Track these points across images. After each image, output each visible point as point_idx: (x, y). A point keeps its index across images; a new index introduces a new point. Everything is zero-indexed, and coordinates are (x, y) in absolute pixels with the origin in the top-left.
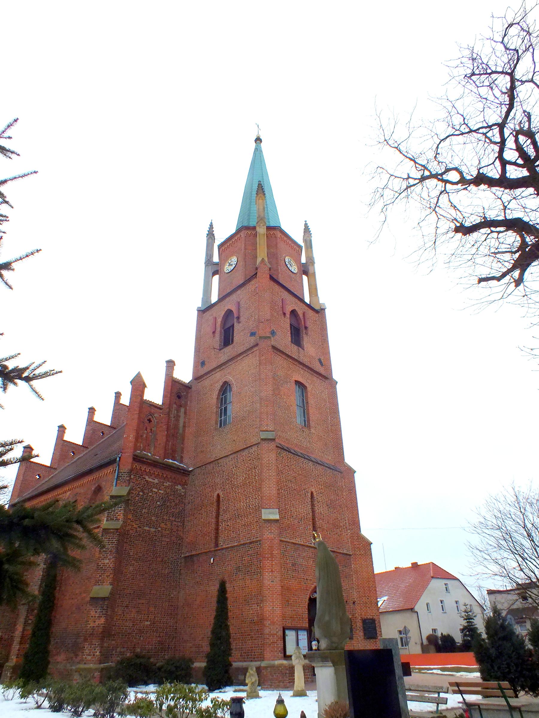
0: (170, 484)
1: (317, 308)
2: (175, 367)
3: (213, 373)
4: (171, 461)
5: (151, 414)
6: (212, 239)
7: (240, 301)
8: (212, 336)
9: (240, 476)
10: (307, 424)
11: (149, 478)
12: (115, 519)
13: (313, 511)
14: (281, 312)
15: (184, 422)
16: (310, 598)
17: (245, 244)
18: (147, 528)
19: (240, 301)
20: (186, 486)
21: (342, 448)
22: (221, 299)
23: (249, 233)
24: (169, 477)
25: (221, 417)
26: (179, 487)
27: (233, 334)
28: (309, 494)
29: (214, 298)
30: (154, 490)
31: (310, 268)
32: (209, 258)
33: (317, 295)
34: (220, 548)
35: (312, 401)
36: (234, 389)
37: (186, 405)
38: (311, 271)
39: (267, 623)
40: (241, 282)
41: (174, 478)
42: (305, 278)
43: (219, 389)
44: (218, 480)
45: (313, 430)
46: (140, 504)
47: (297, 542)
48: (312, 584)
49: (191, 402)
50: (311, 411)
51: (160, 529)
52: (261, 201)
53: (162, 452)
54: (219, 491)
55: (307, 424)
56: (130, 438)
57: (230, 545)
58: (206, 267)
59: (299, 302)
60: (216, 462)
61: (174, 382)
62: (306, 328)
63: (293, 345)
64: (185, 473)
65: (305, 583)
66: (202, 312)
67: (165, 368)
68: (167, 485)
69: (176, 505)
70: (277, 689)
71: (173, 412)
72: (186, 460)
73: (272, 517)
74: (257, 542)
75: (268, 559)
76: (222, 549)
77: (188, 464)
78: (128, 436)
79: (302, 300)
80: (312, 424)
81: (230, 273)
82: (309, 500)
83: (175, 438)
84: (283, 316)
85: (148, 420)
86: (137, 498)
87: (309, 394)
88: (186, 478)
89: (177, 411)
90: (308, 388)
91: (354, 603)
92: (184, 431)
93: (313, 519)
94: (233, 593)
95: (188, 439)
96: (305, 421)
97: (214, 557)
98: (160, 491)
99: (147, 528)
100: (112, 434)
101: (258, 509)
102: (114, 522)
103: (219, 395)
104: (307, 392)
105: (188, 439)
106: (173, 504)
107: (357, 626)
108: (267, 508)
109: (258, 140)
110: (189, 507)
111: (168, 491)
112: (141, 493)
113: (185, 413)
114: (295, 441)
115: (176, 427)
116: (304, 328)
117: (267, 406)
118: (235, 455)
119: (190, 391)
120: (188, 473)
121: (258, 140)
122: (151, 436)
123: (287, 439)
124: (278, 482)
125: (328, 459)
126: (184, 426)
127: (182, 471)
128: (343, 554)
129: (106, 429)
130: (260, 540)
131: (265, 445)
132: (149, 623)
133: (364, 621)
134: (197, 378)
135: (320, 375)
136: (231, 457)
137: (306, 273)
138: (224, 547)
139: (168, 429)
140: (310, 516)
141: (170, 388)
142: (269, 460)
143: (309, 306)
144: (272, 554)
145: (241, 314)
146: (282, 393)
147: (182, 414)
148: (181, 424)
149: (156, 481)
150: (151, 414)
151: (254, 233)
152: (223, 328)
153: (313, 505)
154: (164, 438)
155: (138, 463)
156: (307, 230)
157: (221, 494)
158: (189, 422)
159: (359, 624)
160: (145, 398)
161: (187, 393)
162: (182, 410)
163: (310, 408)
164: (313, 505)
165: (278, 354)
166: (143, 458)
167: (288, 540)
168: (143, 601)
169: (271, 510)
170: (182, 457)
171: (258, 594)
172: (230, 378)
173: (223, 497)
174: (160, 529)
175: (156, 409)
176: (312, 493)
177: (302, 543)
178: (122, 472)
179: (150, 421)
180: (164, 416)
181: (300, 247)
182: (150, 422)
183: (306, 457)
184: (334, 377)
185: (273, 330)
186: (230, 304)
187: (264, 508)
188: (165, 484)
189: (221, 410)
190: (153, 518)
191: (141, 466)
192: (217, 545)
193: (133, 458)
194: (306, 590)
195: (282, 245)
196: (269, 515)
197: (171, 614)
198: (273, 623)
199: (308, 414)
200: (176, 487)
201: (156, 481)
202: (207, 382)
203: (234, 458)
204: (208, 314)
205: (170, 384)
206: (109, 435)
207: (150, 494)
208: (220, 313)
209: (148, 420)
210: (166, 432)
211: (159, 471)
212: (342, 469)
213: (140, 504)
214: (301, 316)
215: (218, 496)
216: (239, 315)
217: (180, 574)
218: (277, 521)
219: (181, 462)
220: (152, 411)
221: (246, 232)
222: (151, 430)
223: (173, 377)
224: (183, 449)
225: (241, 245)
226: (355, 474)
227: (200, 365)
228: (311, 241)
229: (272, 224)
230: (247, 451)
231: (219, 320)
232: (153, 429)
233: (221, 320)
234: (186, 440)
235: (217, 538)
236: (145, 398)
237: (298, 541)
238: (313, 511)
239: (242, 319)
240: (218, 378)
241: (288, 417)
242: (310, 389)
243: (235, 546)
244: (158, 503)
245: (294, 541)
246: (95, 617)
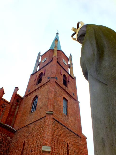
0: (5, 135)
1: (73, 77)
2: (18, 90)
4: (8, 125)
5: (4, 105)
10: (67, 114)
15: (18, 111)
17: (50, 54)
20: (12, 138)
21: (81, 127)
22: (39, 70)
25: (32, 109)
26: (9, 138)
28: (66, 144)
29: (38, 70)
33: (73, 73)
35: (69, 106)
36: (39, 97)
37: (20, 104)
41: (8, 133)
42: (69, 69)
44: (26, 134)
45: (69, 117)
49: (22, 104)
50: (69, 110)
52: (56, 42)
53: (5, 121)
54: (26, 140)
55: (67, 114)
59: (67, 73)
60: (27, 126)
61: (16, 95)
62: (69, 81)
63: (63, 85)
64: (14, 132)
66: (32, 75)
67: (14, 89)
68: (3, 135)
69: (5, 146)
70: (98, 87)
71: (14, 106)
72: (15, 126)
73: (47, 150)
77: (15, 128)
79: (68, 73)
80: (69, 115)
82: (66, 147)
83: (12, 117)
87: (69, 103)
89: (16, 106)
92: (17, 114)
96: (66, 113)
103: (33, 101)
104: (68, 103)
106: (4, 145)
109: (58, 33)
110: (11, 147)
111: (3, 138)
113: (19, 108)
114: (62, 120)
115: (14, 112)
116: (68, 82)
117: (51, 102)
118: (35, 123)
119: (23, 100)
120: (15, 132)
121: (58, 33)
122: (2, 113)
123: (58, 118)
124: (52, 134)
125: (75, 131)
126: (17, 113)
131: (48, 116)
134: (26, 96)
135: (73, 98)
137: (69, 67)
139: (10, 112)
141: (14, 97)
142: (49, 123)
143: (70, 76)
145: (45, 73)
146: (58, 99)
148: (16, 112)
150: (4, 105)
151: (53, 51)
153: (68, 150)
154: (7, 115)
156: (71, 55)
158: (20, 111)
160: (3, 98)
161: (21, 101)
162: (18, 106)
163: (69, 109)
164: (68, 150)
169: (47, 147)
170: (14, 125)
176: (68, 144)
184: (78, 100)
186: (41, 71)
187: (44, 146)
188: (2, 135)
189: (33, 106)
195: (62, 55)
196: (46, 149)
199: (68, 111)
200: (8, 137)
202: (29, 97)
204: (34, 75)
205: (15, 95)
208: (38, 74)
212: (81, 136)
214: (67, 77)
215: (25, 141)
218: (49, 152)
219: (13, 127)
220: (5, 103)
221: (51, 51)
222: (3, 111)
223: (16, 93)
224: (15, 122)
225: (48, 54)
226: (87, 139)
228: (72, 59)
229: (59, 49)
230: (40, 120)
232: (3, 111)
234: (17, 119)
236: (3, 98)
239: (46, 74)
240: (34, 95)
241: (59, 109)
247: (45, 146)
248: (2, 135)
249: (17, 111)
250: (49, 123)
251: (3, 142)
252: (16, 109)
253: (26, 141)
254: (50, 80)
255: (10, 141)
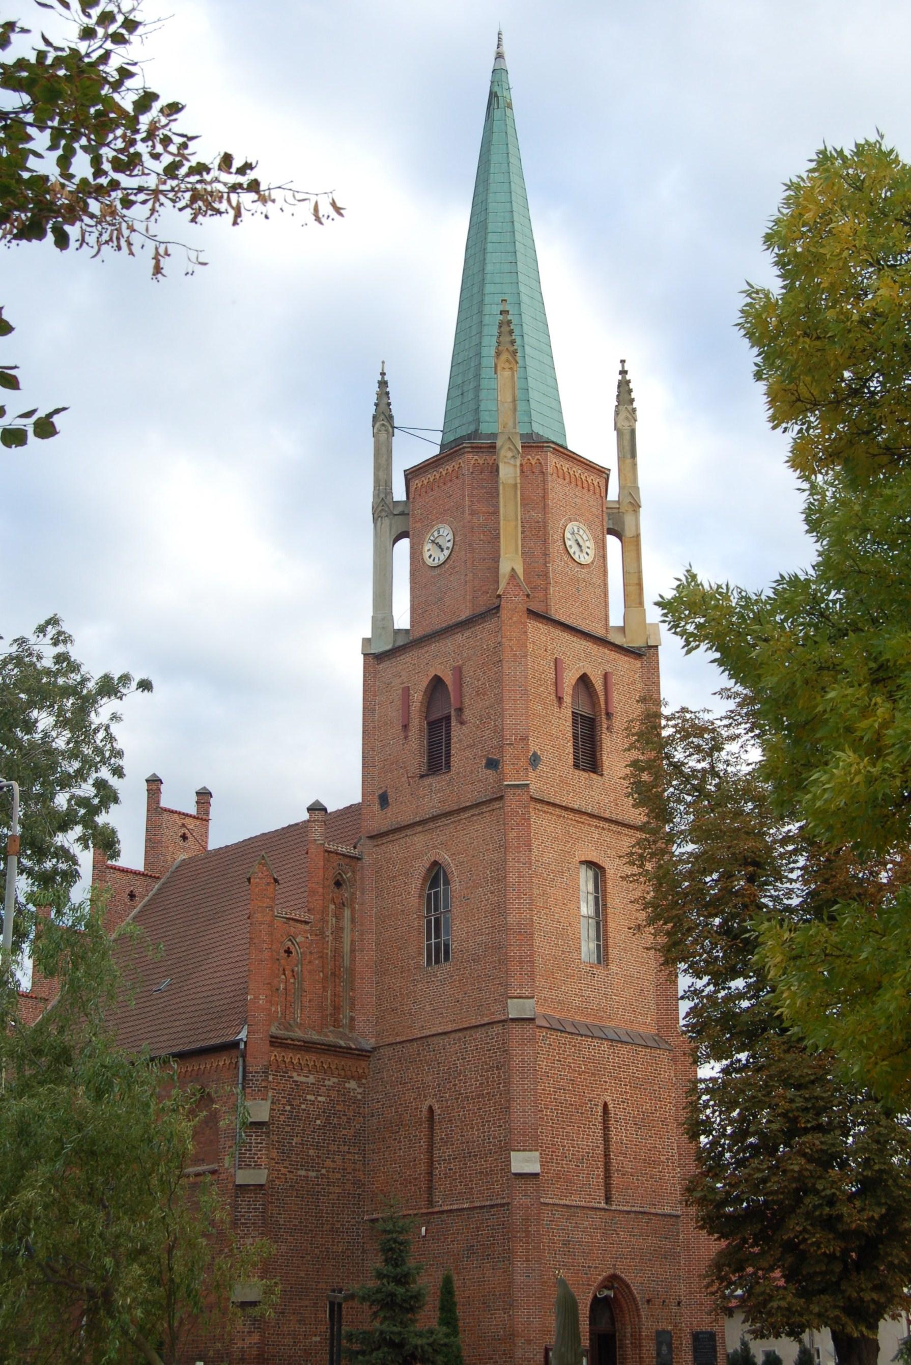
0: (336, 1080)
3: (409, 832)
6: (388, 433)
7: (464, 664)
8: (402, 735)
9: (471, 1078)
11: (299, 1075)
12: (253, 1164)
13: (606, 1139)
14: (553, 697)
15: (353, 942)
16: (595, 1297)
18: (303, 1173)
19: (464, 664)
20: (364, 1081)
23: (481, 462)
24: (333, 1067)
25: (429, 939)
26: (352, 1084)
27: (448, 744)
28: (600, 1109)
30: (309, 1097)
31: (628, 519)
32: (382, 496)
34: (437, 1209)
38: (629, 533)
39: (520, 1341)
40: (464, 615)
42: (613, 544)
43: (422, 874)
45: (613, 967)
46: (288, 1129)
47: (574, 1203)
48: (599, 1275)
51: (324, 1171)
56: (261, 1002)
57: (455, 1207)
58: (375, 521)
64: (363, 1054)
65: (586, 1274)
74: (503, 1205)
75: (521, 1240)
76: (442, 1212)
78: (256, 998)
80: (613, 953)
81: (438, 571)
84: (556, 704)
85: (285, 951)
86: (282, 1118)
88: (364, 1064)
90: (608, 871)
91: (679, 1303)
92: (353, 960)
93: (607, 1155)
94: (463, 1291)
95: (362, 979)
97: (428, 1223)
98: (319, 1098)
99: (303, 1173)
100: (151, 894)
101: (505, 1149)
102: (252, 1171)
104: (604, 881)
105: (362, 979)
107: (682, 1344)
108: (519, 1150)
111: (334, 1094)
112: (288, 1108)
113: (353, 920)
114: (577, 1002)
115: (337, 953)
116: (604, 717)
119: (359, 864)
122: (294, 983)
123: (559, 1002)
126: (353, 951)
127: (357, 1052)
128: (664, 1215)
129: (138, 883)
130: (508, 1204)
132: (318, 1339)
133: (697, 1337)
136: (453, 1035)
138: (446, 1208)
140: (600, 1151)
142: (523, 1061)
144: (527, 1232)
145: (467, 702)
147: (346, 923)
148: (347, 948)
149: (311, 1079)
152: (426, 718)
153: (606, 1128)
155: (279, 1049)
157: (436, 1107)
159: (686, 1342)
162: (347, 913)
163: (610, 917)
164: (606, 1128)
165: (544, 812)
166: (286, 1039)
167: (557, 1202)
168: (307, 1303)
169: (527, 1154)
171: (504, 1294)
172: (445, 857)
173: (440, 1115)
174: (324, 1171)
175: (298, 925)
176: (605, 1105)
177: (583, 1204)
178: (251, 1073)
179: (288, 952)
180: (314, 937)
181: (603, 473)
182: (289, 956)
183: (597, 1033)
185: (535, 754)
187: (514, 1150)
188: (327, 1083)
190: (311, 1152)
191: (283, 1054)
192: (431, 1203)
193: (271, 1041)
194: (588, 1285)
197: (353, 1322)
198: (529, 1342)
200: (347, 1085)
201: (311, 1079)
203: (459, 1039)
206: (147, 898)
207: (303, 1106)
209: (285, 951)
210: (321, 974)
211: (314, 1058)
213: (288, 1129)
215: (431, 1110)
216: (462, 703)
217: (364, 1252)
222: (293, 971)
227: (377, 801)
228: (633, 432)
231: (417, 697)
233: (420, 698)
234: (358, 982)
235: (430, 1190)
237: (574, 1200)
238: (606, 1139)
239: (467, 714)
242: (612, 871)
243: (464, 1209)
244: (318, 1122)
245: (567, 1203)
246: (243, 1332)
247: (521, 1153)
248: (327, 1083)
249: (349, 943)
250: (523, 1061)
251: (338, 1108)
252: (342, 929)
253: (439, 1111)
254: (501, 798)
255: (359, 1097)
